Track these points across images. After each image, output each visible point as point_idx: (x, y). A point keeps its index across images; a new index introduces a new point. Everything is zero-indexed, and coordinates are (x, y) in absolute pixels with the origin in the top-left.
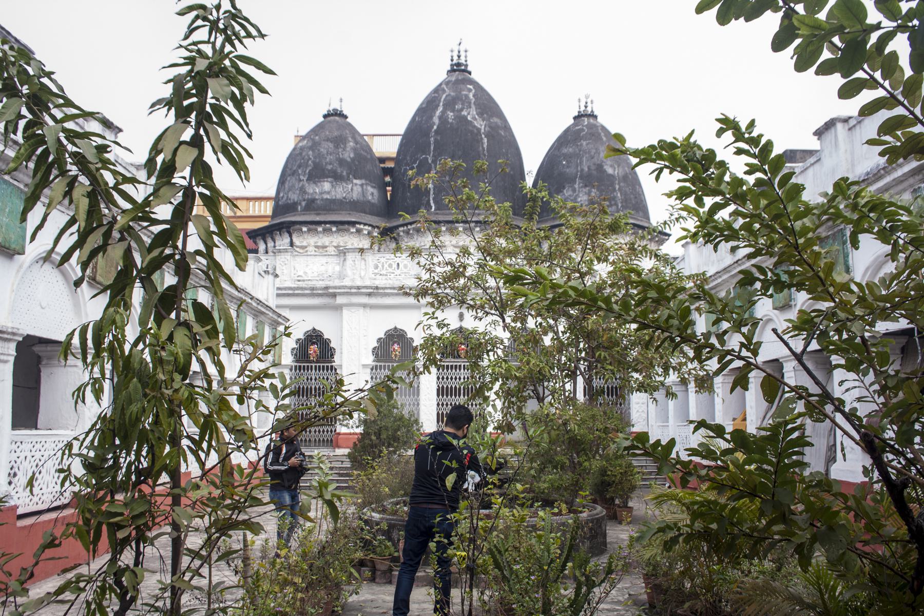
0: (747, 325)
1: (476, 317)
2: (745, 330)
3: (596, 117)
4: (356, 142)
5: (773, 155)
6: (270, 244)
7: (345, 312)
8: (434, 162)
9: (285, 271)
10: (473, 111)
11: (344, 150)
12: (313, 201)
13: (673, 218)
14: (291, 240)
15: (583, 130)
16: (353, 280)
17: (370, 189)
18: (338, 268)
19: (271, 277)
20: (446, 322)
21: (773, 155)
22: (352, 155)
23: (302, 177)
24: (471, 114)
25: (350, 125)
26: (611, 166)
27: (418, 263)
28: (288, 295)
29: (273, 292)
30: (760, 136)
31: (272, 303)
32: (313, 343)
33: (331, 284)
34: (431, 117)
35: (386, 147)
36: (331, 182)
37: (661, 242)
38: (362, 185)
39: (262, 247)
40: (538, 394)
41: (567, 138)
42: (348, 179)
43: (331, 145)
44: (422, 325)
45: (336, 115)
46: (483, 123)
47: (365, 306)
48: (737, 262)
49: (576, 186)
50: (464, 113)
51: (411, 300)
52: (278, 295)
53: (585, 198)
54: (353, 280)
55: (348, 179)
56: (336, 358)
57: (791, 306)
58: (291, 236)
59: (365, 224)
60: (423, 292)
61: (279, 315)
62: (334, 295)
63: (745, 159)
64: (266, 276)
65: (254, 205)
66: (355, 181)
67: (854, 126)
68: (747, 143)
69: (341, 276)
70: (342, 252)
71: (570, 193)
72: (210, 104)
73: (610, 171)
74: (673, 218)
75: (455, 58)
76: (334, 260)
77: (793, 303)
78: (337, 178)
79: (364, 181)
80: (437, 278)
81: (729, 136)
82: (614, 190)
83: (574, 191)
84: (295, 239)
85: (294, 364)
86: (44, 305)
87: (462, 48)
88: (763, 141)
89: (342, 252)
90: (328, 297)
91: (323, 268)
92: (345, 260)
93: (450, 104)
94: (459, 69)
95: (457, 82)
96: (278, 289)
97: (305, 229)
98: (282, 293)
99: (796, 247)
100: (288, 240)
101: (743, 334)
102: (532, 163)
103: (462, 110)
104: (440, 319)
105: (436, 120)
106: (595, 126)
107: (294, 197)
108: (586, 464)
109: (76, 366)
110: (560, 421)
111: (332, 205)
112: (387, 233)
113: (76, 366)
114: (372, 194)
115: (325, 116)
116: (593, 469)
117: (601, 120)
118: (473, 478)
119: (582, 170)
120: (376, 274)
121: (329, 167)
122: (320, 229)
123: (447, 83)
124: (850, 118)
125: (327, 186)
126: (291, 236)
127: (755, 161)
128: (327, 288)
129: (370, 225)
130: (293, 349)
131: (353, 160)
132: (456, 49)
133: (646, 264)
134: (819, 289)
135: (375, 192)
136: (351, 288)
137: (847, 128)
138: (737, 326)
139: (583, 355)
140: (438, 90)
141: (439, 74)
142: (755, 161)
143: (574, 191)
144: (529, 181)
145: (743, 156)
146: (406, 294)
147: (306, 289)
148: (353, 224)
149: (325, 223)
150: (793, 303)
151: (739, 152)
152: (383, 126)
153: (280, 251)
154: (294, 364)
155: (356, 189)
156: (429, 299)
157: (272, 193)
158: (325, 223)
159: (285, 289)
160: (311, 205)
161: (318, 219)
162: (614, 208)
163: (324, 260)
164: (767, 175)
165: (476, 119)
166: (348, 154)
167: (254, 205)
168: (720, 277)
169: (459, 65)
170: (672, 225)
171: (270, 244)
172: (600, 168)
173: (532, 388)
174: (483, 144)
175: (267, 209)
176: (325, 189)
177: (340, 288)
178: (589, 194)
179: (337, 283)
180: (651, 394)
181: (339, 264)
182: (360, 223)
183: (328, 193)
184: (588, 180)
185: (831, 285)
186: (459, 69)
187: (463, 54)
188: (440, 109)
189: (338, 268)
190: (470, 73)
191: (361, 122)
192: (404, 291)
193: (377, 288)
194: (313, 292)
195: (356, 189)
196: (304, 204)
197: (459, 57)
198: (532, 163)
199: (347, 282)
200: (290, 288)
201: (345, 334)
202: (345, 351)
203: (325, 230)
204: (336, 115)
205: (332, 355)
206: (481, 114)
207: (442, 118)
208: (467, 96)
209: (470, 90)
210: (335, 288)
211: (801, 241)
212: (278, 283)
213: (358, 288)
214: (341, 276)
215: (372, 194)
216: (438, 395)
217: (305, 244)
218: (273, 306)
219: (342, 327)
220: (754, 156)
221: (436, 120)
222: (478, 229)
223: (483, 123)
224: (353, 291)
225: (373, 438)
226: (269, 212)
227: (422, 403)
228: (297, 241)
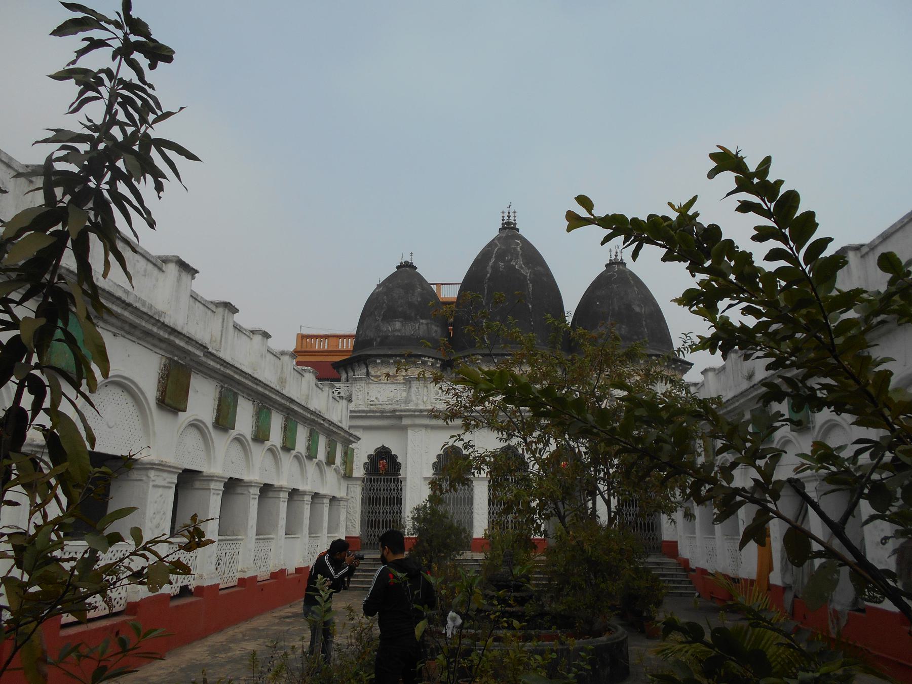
0: (765, 457)
1: (501, 439)
2: (761, 463)
3: (625, 264)
5: (798, 214)
6: (351, 374)
7: (410, 431)
9: (360, 397)
12: (387, 337)
13: (686, 345)
14: (368, 371)
15: (613, 275)
16: (417, 404)
17: (434, 328)
18: (404, 394)
19: (344, 402)
20: (471, 443)
21: (798, 214)
24: (518, 264)
26: (639, 305)
27: (441, 388)
28: (362, 417)
29: (346, 415)
30: (780, 183)
31: (345, 425)
32: (382, 459)
33: (398, 407)
35: (450, 293)
36: (402, 322)
37: (685, 371)
38: (427, 324)
39: (344, 376)
40: (560, 512)
45: (407, 268)
46: (529, 271)
47: (426, 427)
48: (753, 386)
51: (441, 422)
52: (351, 417)
54: (417, 404)
56: (402, 471)
57: (809, 428)
58: (367, 367)
59: (429, 357)
60: (452, 415)
61: (351, 435)
62: (400, 418)
63: (755, 220)
64: (341, 401)
65: (343, 342)
66: (421, 321)
67: (867, 253)
68: (757, 194)
69: (407, 401)
70: (408, 381)
73: (637, 309)
74: (686, 345)
75: (506, 218)
76: (400, 387)
77: (811, 425)
78: (406, 318)
79: (429, 321)
80: (463, 402)
81: (728, 179)
84: (370, 370)
85: (365, 477)
86: (111, 424)
87: (511, 210)
88: (783, 190)
89: (408, 381)
90: (395, 419)
91: (392, 394)
92: (410, 387)
93: (501, 256)
94: (509, 228)
96: (351, 411)
97: (379, 361)
98: (355, 415)
99: (832, 349)
100: (365, 371)
101: (758, 469)
102: (570, 305)
103: (511, 260)
104: (466, 441)
105: (489, 270)
107: (371, 334)
108: (603, 585)
109: (141, 480)
110: (574, 543)
111: (402, 341)
112: (447, 365)
113: (141, 480)
114: (435, 330)
115: (398, 267)
116: (614, 588)
118: (454, 619)
120: (436, 399)
121: (400, 309)
122: (391, 361)
123: (497, 238)
124: (862, 245)
125: (398, 325)
126: (367, 367)
127: (770, 223)
128: (394, 411)
129: (433, 358)
130: (365, 464)
132: (506, 211)
133: (661, 388)
134: (869, 411)
135: (439, 330)
136: (414, 411)
137: (859, 255)
138: (751, 459)
139: (602, 475)
140: (491, 245)
141: (492, 231)
142: (770, 223)
144: (569, 320)
145: (751, 214)
146: (436, 417)
147: (376, 412)
148: (419, 356)
149: (396, 356)
150: (811, 425)
151: (745, 207)
153: (355, 380)
154: (365, 477)
155: (421, 327)
156: (459, 422)
157: (354, 332)
158: (396, 356)
159: (359, 411)
160: (385, 341)
161: (390, 352)
163: (393, 387)
164: (787, 243)
166: (416, 299)
167: (343, 342)
168: (738, 401)
169: (508, 223)
170: (685, 352)
171: (351, 374)
173: (552, 505)
175: (349, 345)
176: (396, 326)
177: (405, 411)
179: (403, 407)
180: (669, 515)
181: (405, 390)
182: (425, 356)
183: (399, 331)
185: (886, 406)
186: (509, 228)
187: (512, 215)
188: (493, 260)
189: (404, 394)
190: (518, 230)
191: (429, 272)
192: (434, 414)
194: (382, 414)
195: (421, 327)
196: (378, 340)
197: (509, 217)
198: (570, 305)
199: (411, 406)
200: (363, 411)
201: (409, 448)
202: (409, 466)
204: (407, 268)
205: (399, 470)
207: (495, 268)
208: (515, 249)
209: (518, 244)
210: (401, 411)
211: (839, 341)
212: (352, 407)
213: (421, 411)
214: (407, 401)
215: (436, 331)
216: (489, 505)
217: (379, 373)
218: (346, 427)
219: (407, 445)
220: (766, 214)
221: (489, 270)
223: (529, 271)
224: (417, 413)
225: (425, 544)
226: (350, 347)
227: (475, 511)
228: (372, 372)
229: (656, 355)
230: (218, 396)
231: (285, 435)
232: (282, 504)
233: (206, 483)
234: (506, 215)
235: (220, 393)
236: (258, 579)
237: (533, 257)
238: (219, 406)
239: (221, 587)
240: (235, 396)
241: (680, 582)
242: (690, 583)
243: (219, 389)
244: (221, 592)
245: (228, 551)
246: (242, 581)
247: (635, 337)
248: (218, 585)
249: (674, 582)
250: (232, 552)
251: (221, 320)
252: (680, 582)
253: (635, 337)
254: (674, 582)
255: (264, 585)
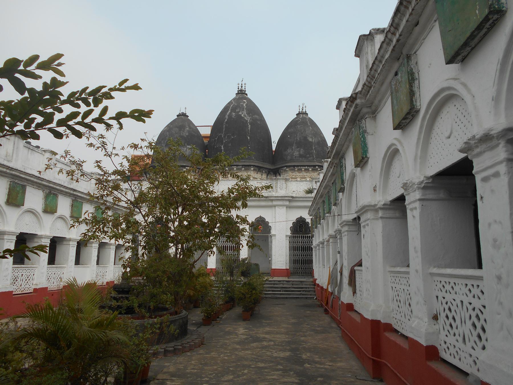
4: (190, 128)
7: (277, 208)
8: (224, 137)
10: (245, 112)
11: (183, 131)
15: (299, 120)
22: (187, 134)
23: (163, 145)
24: (243, 113)
25: (310, 119)
26: (311, 137)
34: (225, 116)
35: (205, 131)
41: (292, 125)
42: (185, 145)
43: (177, 129)
44: (87, 213)
45: (183, 116)
46: (249, 118)
49: (294, 148)
50: (240, 113)
53: (298, 153)
55: (185, 145)
71: (291, 151)
72: (54, 114)
73: (310, 140)
82: (312, 149)
83: (292, 150)
93: (234, 109)
94: (241, 93)
95: (239, 99)
102: (275, 137)
103: (239, 112)
105: (227, 117)
106: (305, 118)
117: (310, 116)
119: (297, 140)
123: (234, 99)
131: (187, 136)
141: (232, 95)
143: (292, 150)
152: (204, 121)
162: (311, 158)
165: (245, 116)
166: (185, 134)
169: (241, 90)
172: (305, 138)
174: (248, 128)
178: (299, 151)
184: (299, 145)
186: (241, 93)
187: (243, 85)
193: (292, 197)
197: (242, 87)
198: (275, 137)
203: (305, 170)
204: (183, 116)
205: (270, 230)
206: (248, 114)
221: (227, 117)
222: (243, 169)
223: (249, 118)
229: (318, 166)
230: (8, 186)
231: (72, 210)
232: (71, 249)
233: (2, 236)
234: (240, 86)
235: (10, 185)
236: (48, 290)
237: (253, 110)
238: (9, 192)
239: (14, 293)
240: (24, 188)
241: (309, 291)
242: (315, 291)
243: (9, 183)
244: (14, 296)
245: (24, 274)
246: (35, 290)
247: (308, 156)
248: (12, 292)
249: (306, 291)
250: (59, 273)
251: (13, 144)
252: (309, 291)
253: (308, 156)
254: (306, 291)
255: (54, 293)
